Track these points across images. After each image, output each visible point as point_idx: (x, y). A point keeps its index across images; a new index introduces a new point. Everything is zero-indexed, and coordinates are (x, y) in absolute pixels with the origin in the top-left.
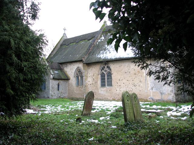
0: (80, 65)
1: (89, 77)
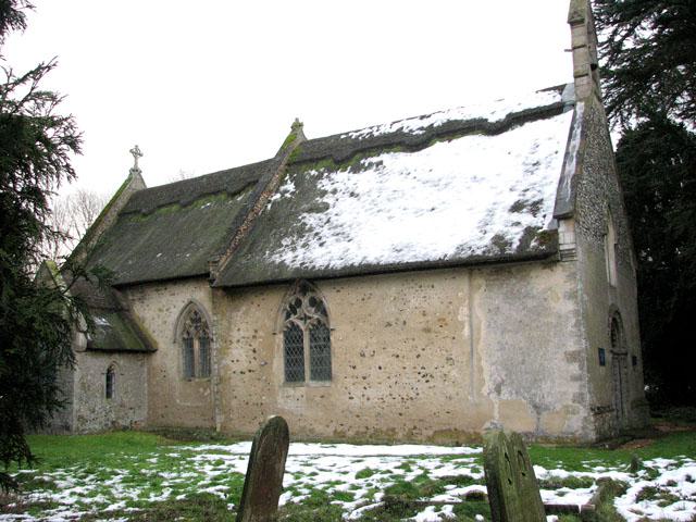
0: (200, 295)
1: (235, 345)
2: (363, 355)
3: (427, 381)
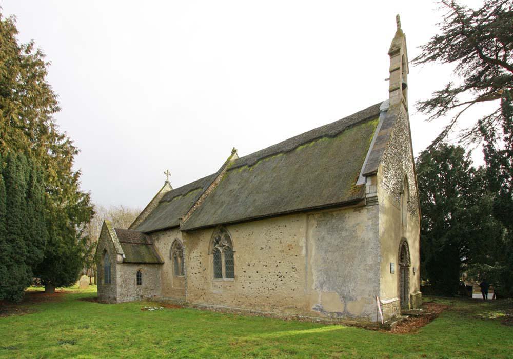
0: (179, 236)
1: (192, 260)
2: (249, 265)
3: (281, 280)
